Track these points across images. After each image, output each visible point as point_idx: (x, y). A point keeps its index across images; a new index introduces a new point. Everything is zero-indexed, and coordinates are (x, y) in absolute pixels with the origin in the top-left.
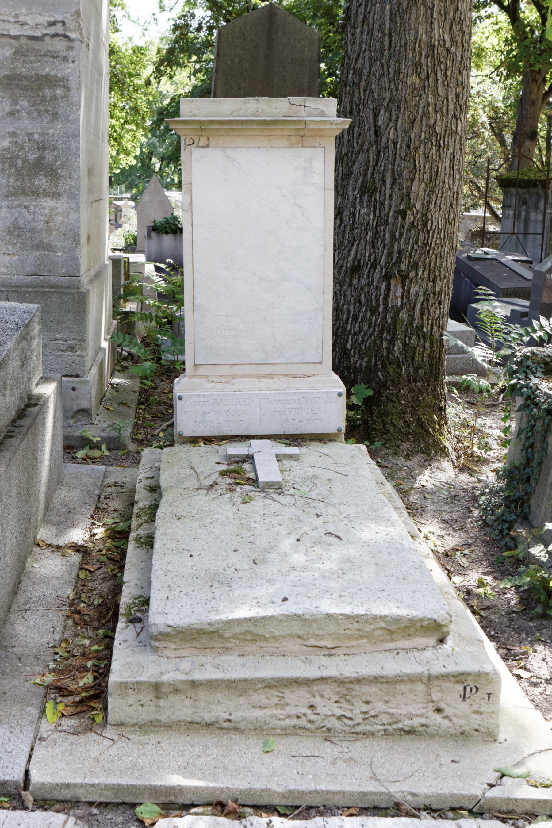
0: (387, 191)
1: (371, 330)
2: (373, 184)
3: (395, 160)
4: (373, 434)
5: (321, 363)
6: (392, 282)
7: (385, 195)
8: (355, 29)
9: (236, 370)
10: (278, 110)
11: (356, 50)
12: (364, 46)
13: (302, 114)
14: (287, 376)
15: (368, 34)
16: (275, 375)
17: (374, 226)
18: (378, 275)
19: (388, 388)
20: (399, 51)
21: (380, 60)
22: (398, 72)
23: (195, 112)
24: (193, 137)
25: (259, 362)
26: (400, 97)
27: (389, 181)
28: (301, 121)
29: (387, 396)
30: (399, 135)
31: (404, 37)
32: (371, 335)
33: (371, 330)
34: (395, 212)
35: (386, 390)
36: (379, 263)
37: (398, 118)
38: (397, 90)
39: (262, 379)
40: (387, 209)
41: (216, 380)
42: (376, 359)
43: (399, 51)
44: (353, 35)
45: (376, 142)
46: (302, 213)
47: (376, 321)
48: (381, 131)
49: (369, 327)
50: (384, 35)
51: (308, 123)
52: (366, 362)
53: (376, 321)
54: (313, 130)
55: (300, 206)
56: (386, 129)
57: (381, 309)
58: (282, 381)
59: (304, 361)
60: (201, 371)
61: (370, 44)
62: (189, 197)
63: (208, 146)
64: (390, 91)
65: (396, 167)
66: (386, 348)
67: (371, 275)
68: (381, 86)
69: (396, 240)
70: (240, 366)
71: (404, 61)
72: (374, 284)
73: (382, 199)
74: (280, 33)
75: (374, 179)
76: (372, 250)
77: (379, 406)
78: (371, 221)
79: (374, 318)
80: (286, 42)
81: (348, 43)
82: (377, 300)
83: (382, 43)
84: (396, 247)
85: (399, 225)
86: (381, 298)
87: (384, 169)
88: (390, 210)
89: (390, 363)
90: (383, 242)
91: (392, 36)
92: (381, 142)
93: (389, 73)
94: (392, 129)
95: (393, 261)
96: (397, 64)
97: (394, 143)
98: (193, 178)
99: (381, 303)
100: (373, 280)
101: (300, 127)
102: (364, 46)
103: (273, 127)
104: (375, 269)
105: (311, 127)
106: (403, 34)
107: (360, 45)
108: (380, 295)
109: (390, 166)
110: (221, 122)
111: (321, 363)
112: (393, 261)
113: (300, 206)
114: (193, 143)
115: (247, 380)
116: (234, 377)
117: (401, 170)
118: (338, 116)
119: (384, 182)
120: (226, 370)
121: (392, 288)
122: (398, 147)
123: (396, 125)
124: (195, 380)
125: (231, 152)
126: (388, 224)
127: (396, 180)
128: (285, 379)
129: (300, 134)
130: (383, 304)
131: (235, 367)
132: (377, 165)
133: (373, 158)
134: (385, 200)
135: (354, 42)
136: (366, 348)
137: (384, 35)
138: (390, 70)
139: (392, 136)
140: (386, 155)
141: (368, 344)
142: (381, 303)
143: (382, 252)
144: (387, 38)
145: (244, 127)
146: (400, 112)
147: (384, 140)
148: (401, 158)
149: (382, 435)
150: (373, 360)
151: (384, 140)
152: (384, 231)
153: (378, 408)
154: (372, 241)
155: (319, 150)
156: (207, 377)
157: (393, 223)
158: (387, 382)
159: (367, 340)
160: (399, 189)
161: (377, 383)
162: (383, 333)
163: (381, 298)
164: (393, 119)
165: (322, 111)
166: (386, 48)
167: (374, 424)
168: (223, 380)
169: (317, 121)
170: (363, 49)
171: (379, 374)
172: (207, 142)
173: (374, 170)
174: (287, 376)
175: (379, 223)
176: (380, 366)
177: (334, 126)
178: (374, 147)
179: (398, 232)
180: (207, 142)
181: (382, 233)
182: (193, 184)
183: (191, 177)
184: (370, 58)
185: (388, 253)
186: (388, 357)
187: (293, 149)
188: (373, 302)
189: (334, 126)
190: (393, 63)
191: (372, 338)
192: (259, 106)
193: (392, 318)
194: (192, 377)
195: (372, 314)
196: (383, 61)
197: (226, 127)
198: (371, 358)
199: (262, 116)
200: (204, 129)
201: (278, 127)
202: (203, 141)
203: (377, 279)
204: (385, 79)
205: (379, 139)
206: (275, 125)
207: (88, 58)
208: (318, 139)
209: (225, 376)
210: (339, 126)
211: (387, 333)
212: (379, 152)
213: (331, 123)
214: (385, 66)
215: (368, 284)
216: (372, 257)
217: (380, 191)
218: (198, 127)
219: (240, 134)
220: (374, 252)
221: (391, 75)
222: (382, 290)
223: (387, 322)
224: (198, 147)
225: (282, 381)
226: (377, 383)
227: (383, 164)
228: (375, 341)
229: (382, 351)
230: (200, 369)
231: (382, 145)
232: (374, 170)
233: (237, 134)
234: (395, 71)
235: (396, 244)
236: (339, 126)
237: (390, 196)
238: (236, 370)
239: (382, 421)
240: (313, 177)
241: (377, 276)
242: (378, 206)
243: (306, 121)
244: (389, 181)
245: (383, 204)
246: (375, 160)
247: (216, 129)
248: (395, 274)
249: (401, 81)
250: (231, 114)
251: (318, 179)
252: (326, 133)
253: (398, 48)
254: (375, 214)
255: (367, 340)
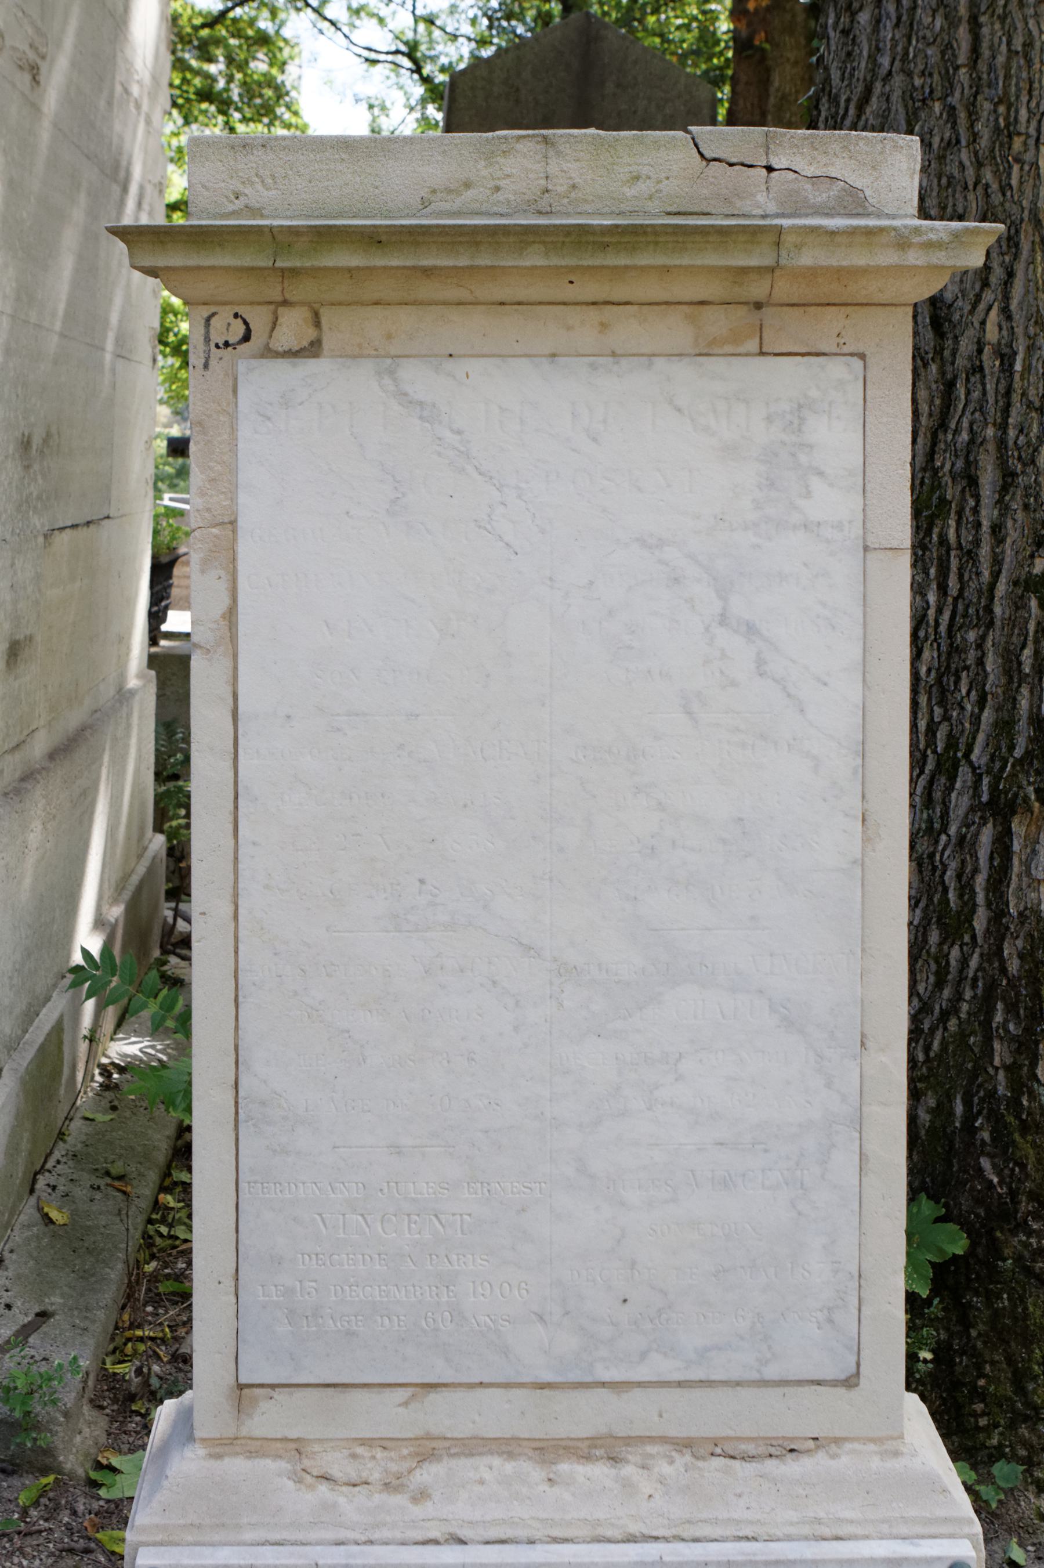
0: (984, 512)
1: (947, 993)
2: (932, 490)
3: (1006, 411)
4: (976, 1415)
5: (851, 1382)
6: (1017, 826)
7: (978, 525)
8: (853, 15)
9: (442, 1415)
10: (643, 187)
11: (861, 73)
12: (885, 61)
13: (760, 201)
14: (686, 1445)
15: (897, 25)
16: (629, 1441)
17: (943, 629)
18: (965, 801)
19: (1023, 1226)
20: (1007, 67)
21: (943, 99)
22: (1005, 133)
23: (257, 194)
24: (241, 310)
25: (548, 1377)
26: (1015, 209)
27: (988, 478)
28: (754, 233)
29: (1019, 1259)
30: (1019, 331)
31: (1020, 25)
32: (945, 1016)
33: (947, 993)
34: (1016, 583)
35: (1014, 1232)
36: (967, 755)
37: (1010, 274)
38: (1005, 188)
39: (564, 1467)
40: (986, 574)
41: (337, 1464)
42: (967, 1103)
43: (1007, 67)
44: (845, 32)
45: (939, 351)
46: (760, 662)
47: (964, 962)
48: (956, 317)
49: (940, 984)
50: (952, 22)
51: (789, 240)
52: (930, 1111)
53: (964, 962)
54: (813, 273)
55: (751, 630)
56: (972, 312)
57: (980, 922)
58: (662, 1481)
59: (772, 1372)
60: (269, 1419)
61: (906, 53)
62: (223, 586)
63: (313, 349)
64: (980, 190)
65: (1012, 433)
66: (1007, 1068)
67: (937, 795)
68: (951, 177)
69: (1022, 678)
70: (459, 1395)
71: (1024, 99)
72: (953, 830)
73: (967, 537)
74: (610, 87)
75: (935, 471)
76: (938, 711)
77: (990, 1297)
78: (931, 612)
79: (955, 953)
80: (623, 107)
81: (828, 58)
82: (966, 888)
83: (949, 46)
84: (1024, 704)
85: (1032, 627)
86: (980, 880)
87: (972, 441)
88: (996, 575)
89: (1024, 1128)
90: (978, 684)
91: (980, 26)
92: (954, 354)
93: (975, 137)
94: (994, 313)
95: (1018, 753)
96: (1002, 109)
97: (1002, 356)
98: (243, 498)
99: (980, 898)
100: (945, 815)
101: (754, 262)
102: (885, 61)
103: (623, 260)
104: (952, 779)
105: (806, 259)
106: (1017, 16)
107: (872, 59)
108: (976, 871)
109: (990, 432)
110: (374, 239)
111: (851, 1382)
112: (1018, 753)
113: (751, 630)
114: (247, 338)
115: (491, 1468)
116: (428, 1449)
117: (1029, 444)
118: (924, 213)
119: (972, 482)
120: (388, 1415)
121: (1016, 847)
122: (1018, 367)
123: (1007, 298)
124: (236, 1466)
125: (417, 378)
126: (991, 624)
127: (1014, 475)
128: (672, 1468)
129: (750, 293)
130: (989, 905)
131: (433, 1397)
132: (943, 425)
133: (931, 403)
134: (977, 542)
135: (849, 54)
136: (928, 1059)
137: (952, 22)
138: (979, 126)
139: (992, 334)
140: (976, 395)
141: (936, 1045)
142: (980, 898)
143: (976, 720)
144: (963, 33)
145: (484, 260)
146: (1016, 257)
147: (966, 346)
148: (1030, 405)
149: (1012, 1426)
150: (959, 1108)
151: (966, 346)
152: (980, 646)
153: (989, 1304)
154: (939, 680)
155: (840, 371)
156: (298, 1447)
157: (1011, 622)
158: (1016, 1202)
159: (933, 1030)
160: (1026, 507)
161: (978, 1201)
162: (990, 1012)
163: (980, 880)
164: (993, 280)
165: (853, 191)
166: (962, 59)
167: (979, 1367)
168: (375, 1467)
169: (833, 233)
170: (883, 71)
171: (985, 1163)
172: (311, 333)
173: (934, 443)
174: (686, 1445)
175: (959, 620)
176: (986, 1135)
177: (914, 258)
178: (934, 368)
179: (1027, 652)
180: (311, 333)
181: (972, 655)
182: (241, 523)
183: (232, 493)
184: (909, 95)
185: (996, 724)
186: (1014, 1103)
187: (716, 365)
188: (952, 895)
189: (914, 258)
190: (987, 106)
191: (953, 1024)
192: (553, 168)
193: (1021, 956)
194: (223, 1447)
195: (950, 935)
196: (955, 99)
197: (395, 261)
198: (950, 1099)
199: (568, 214)
200: (294, 272)
201: (644, 259)
202: (292, 328)
203: (961, 812)
204: (964, 155)
205: (949, 343)
206: (633, 249)
207: (35, 108)
208: (833, 320)
209: (384, 1444)
210: (939, 258)
211: (1007, 1011)
212: (950, 386)
213: (902, 241)
214: (962, 115)
215: (930, 829)
216: (941, 735)
217: (960, 514)
218: (264, 262)
219: (463, 294)
220: (946, 718)
221: (984, 142)
222: (983, 854)
223: (1003, 970)
224: (269, 353)
225: (662, 1481)
226: (978, 1201)
227: (965, 424)
228: (963, 1036)
229: (992, 1078)
230: (264, 1405)
231: (961, 362)
232: (934, 443)
233: (453, 293)
234: (997, 130)
235: (1025, 691)
236: (939, 258)
237: (997, 529)
238: (442, 1415)
239: (1010, 1360)
240: (808, 494)
241: (960, 803)
242: (954, 563)
243: (779, 230)
244: (988, 478)
245: (970, 555)
246: (936, 411)
247: (350, 272)
248: (1026, 799)
249: (1017, 160)
250: (425, 203)
251: (834, 503)
252: (871, 288)
253: (1001, 59)
254: (943, 589)
255: (933, 1030)
